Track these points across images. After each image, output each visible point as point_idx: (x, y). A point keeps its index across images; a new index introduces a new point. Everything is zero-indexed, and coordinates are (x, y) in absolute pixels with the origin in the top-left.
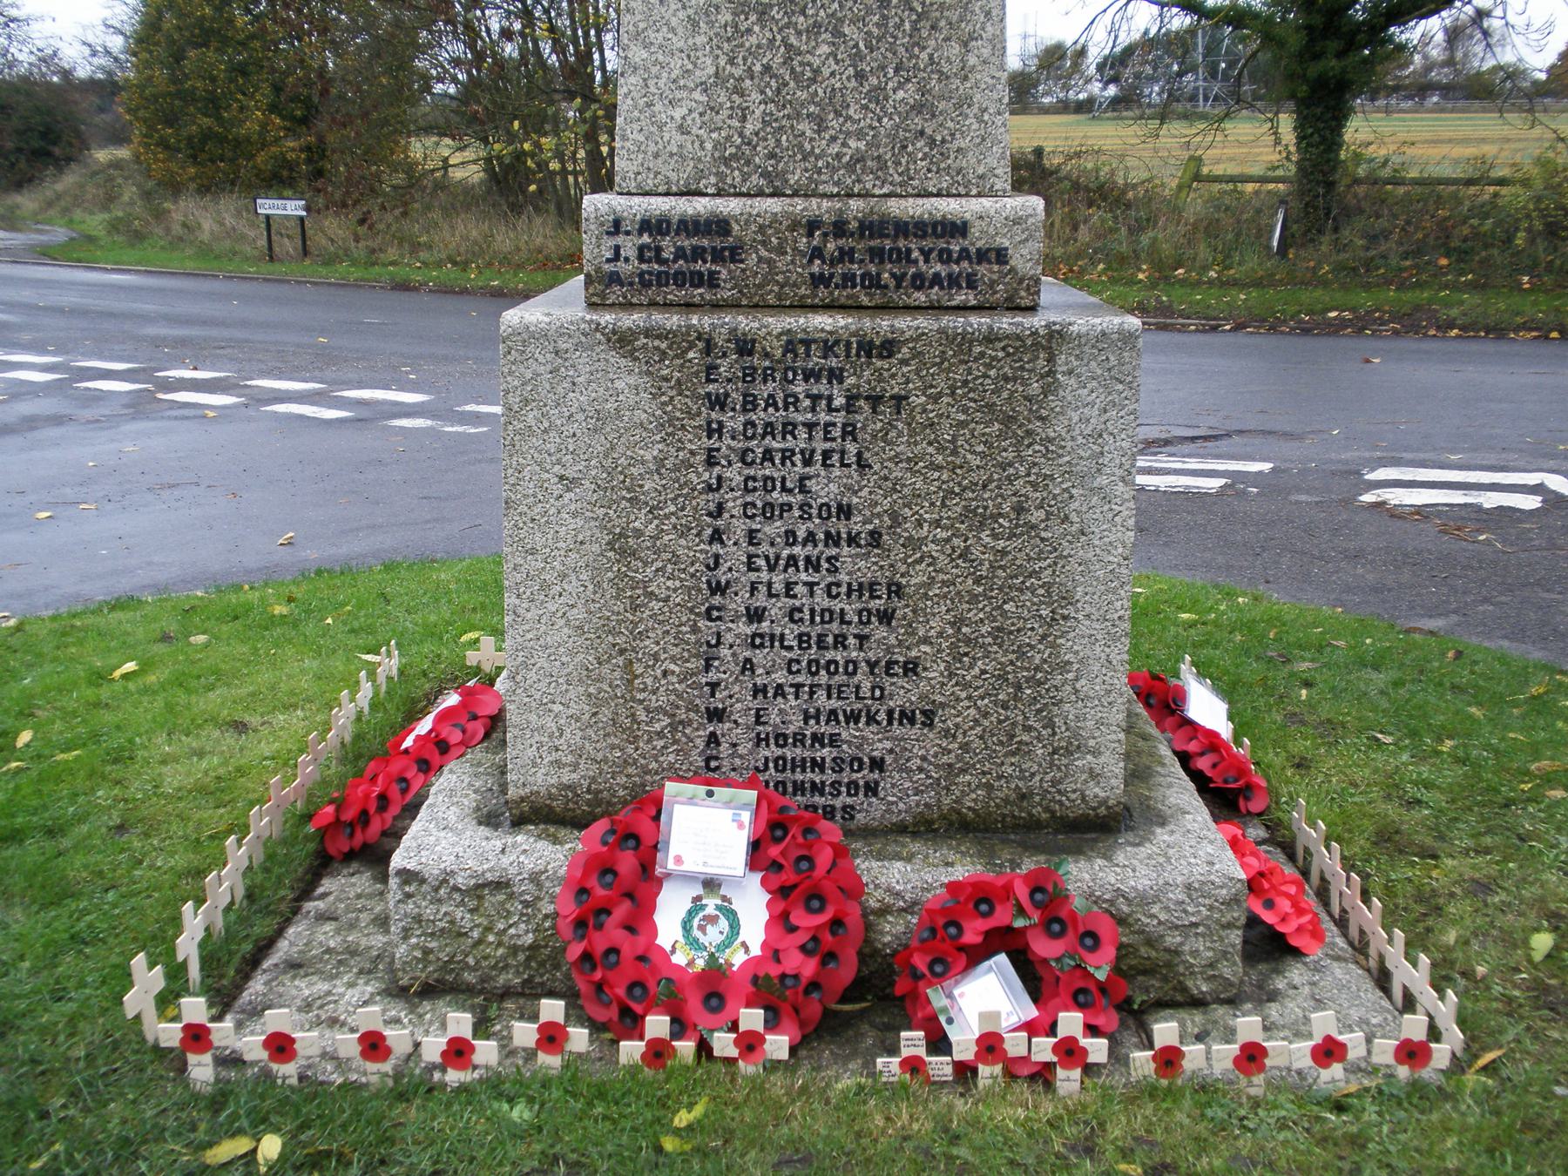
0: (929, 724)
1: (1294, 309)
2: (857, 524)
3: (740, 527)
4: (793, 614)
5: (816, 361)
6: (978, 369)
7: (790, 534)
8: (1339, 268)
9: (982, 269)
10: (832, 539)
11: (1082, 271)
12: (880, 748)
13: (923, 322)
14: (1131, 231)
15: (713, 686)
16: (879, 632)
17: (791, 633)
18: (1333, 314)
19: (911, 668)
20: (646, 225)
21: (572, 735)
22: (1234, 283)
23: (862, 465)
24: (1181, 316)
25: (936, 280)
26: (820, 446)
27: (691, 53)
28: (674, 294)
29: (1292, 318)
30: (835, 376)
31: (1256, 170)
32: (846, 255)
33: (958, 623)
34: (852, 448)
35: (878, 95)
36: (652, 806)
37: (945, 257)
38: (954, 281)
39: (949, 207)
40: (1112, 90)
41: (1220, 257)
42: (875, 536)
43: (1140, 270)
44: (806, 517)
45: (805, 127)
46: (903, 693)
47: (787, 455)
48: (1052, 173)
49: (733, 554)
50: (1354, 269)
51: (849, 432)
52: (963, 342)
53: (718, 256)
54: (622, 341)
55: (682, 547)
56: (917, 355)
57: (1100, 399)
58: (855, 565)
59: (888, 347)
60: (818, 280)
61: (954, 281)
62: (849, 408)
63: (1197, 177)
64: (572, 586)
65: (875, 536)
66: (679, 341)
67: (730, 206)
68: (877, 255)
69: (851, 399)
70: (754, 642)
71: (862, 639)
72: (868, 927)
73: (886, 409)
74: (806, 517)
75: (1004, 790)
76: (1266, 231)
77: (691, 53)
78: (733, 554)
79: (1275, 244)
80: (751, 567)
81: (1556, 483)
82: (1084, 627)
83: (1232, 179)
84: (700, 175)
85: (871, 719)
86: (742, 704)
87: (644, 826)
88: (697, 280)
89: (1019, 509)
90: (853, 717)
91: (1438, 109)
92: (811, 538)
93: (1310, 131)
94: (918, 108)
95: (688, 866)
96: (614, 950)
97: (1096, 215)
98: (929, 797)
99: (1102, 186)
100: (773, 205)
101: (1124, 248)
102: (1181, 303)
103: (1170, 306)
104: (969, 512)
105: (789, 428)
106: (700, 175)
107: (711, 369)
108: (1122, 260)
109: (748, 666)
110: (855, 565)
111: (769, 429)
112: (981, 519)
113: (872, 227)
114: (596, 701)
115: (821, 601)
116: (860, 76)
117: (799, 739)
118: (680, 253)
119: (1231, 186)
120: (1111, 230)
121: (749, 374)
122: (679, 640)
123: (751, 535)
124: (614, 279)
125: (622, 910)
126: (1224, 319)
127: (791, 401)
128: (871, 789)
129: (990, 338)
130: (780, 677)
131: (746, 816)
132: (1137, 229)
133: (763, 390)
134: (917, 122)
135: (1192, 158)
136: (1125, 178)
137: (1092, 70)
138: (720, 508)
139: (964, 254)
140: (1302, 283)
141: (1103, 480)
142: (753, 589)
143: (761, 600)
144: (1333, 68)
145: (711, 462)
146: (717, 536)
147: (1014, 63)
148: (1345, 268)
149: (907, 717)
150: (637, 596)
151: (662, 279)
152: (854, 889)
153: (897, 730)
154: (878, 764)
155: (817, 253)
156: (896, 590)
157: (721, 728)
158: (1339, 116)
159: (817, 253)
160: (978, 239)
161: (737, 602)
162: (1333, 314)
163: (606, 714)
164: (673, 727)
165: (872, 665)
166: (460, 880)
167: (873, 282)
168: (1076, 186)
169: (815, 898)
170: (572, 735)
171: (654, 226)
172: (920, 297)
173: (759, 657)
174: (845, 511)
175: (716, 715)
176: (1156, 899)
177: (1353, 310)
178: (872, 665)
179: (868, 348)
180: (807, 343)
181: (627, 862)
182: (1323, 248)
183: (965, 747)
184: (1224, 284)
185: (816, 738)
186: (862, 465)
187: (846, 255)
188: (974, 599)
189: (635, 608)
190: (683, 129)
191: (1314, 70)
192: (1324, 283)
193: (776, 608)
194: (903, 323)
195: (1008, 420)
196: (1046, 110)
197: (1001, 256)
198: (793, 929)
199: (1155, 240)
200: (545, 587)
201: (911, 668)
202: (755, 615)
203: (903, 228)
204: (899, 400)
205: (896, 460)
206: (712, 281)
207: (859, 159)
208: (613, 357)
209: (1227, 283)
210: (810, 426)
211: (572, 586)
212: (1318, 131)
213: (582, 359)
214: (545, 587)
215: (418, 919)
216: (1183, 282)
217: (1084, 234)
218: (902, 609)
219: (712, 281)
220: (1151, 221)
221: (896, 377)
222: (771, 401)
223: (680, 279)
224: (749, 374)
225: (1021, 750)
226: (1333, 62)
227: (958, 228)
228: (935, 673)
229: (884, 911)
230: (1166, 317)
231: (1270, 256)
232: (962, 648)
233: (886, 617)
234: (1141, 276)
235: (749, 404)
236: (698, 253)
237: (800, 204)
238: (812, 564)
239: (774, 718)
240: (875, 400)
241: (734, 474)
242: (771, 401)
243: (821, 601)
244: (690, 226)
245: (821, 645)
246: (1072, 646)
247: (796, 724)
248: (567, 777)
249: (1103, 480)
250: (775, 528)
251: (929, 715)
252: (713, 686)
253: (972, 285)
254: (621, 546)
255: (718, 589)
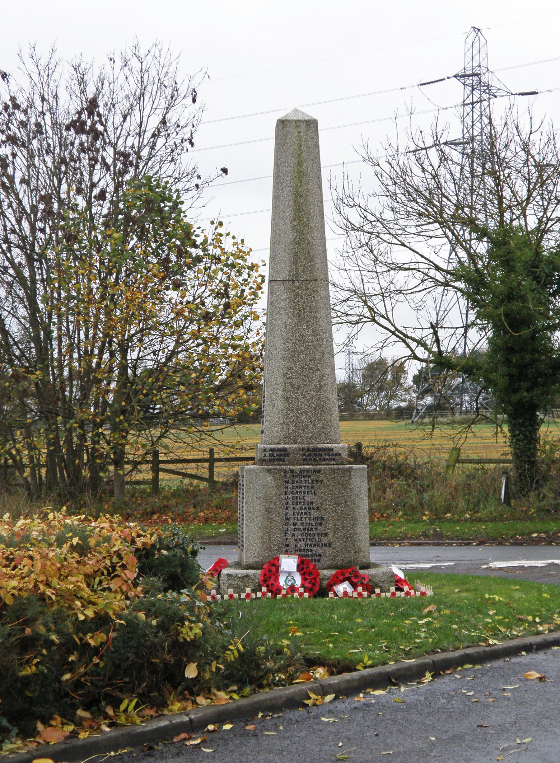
0: (330, 546)
1: (511, 533)
2: (314, 505)
3: (291, 506)
4: (302, 524)
5: (306, 474)
6: (336, 475)
7: (301, 508)
8: (540, 510)
9: (336, 457)
10: (310, 509)
11: (389, 517)
12: (320, 551)
13: (325, 467)
14: (419, 492)
15: (287, 539)
16: (319, 527)
17: (302, 528)
18: (535, 535)
19: (326, 535)
20: (271, 450)
21: (258, 551)
22: (480, 520)
23: (315, 494)
24: (448, 539)
25: (327, 459)
26: (307, 490)
27: (279, 418)
28: (276, 463)
29: (512, 538)
30: (309, 477)
31: (495, 456)
32: (310, 455)
33: (335, 525)
34: (313, 491)
35: (315, 425)
36: (278, 559)
37: (329, 455)
38: (331, 460)
39: (329, 446)
40: (429, 400)
41: (471, 506)
42: (318, 508)
43: (424, 514)
44: (304, 504)
45: (301, 431)
46: (325, 540)
47: (300, 492)
48: (368, 459)
49: (290, 512)
50: (548, 511)
51: (312, 487)
52: (333, 470)
53: (285, 455)
54: (269, 471)
55: (280, 511)
56: (324, 472)
57: (360, 480)
58: (314, 514)
59: (319, 471)
60: (304, 460)
61: (331, 460)
62: (312, 483)
63: (458, 461)
64: (259, 519)
65: (318, 508)
66: (280, 471)
67: (287, 446)
68: (316, 455)
69: (313, 481)
70: (295, 530)
71: (316, 529)
72: (321, 582)
73: (319, 483)
74: (304, 504)
75: (346, 561)
76: (497, 491)
77: (279, 418)
78: (290, 512)
79: (502, 497)
80: (294, 514)
81: (557, 561)
82: (360, 526)
83: (479, 462)
84: (280, 440)
85: (318, 546)
86: (292, 543)
87: (276, 562)
88: (281, 460)
89: (346, 502)
90: (315, 545)
91: (484, 424)
92: (305, 508)
93: (517, 432)
94: (322, 427)
95: (285, 570)
96: (272, 584)
97: (398, 483)
98: (331, 562)
99: (400, 466)
100: (295, 446)
101: (414, 502)
102: (447, 532)
103: (442, 533)
104: (336, 503)
105: (301, 487)
106: (280, 440)
107: (286, 476)
108: (413, 509)
109: (294, 535)
110: (314, 514)
111: (297, 487)
112: (338, 504)
113: (315, 449)
114: (263, 543)
115: (308, 521)
116: (311, 422)
117: (304, 550)
118: (277, 455)
119: (478, 466)
120: (406, 492)
121: (293, 476)
122: (280, 530)
123: (294, 508)
124: (264, 460)
125: (273, 578)
126: (473, 539)
127: (301, 482)
128: (319, 561)
129: (338, 469)
130: (300, 537)
131: (296, 560)
132: (422, 490)
133: (296, 480)
134: (322, 430)
135: (454, 449)
136: (415, 462)
137: (409, 382)
138: (288, 503)
139: (333, 454)
140: (519, 519)
141: (361, 496)
142: (294, 519)
143: (296, 521)
144: (525, 397)
145: (286, 494)
146: (287, 508)
147: (341, 376)
148: (543, 510)
149: (325, 545)
150: (271, 521)
151: (274, 460)
152: (318, 574)
153: (324, 548)
154: (320, 555)
155: (304, 455)
156: (322, 519)
157: (288, 548)
158: (534, 424)
159: (304, 455)
160: (335, 451)
161: (291, 522)
162: (535, 535)
163: (265, 545)
164: (279, 548)
165: (318, 534)
166: (239, 576)
167: (315, 460)
168: (384, 466)
169: (310, 573)
170: (258, 551)
171: (272, 450)
172: (324, 463)
173: (296, 533)
174: (312, 503)
175: (287, 545)
176: (377, 576)
177: (546, 532)
178: (318, 534)
179: (315, 471)
180: (304, 471)
181: (273, 569)
182: (531, 499)
183: (338, 551)
184: (473, 521)
185: (308, 550)
186: (315, 494)
187: (310, 455)
188: (338, 520)
189: (271, 523)
190: (277, 432)
191: (515, 398)
192: (532, 519)
193: (299, 523)
194: (321, 467)
195: (343, 485)
196: (370, 417)
197: (340, 455)
198: (307, 579)
199: (432, 497)
200: (253, 519)
201: (326, 535)
202: (295, 524)
203: (321, 450)
204: (322, 481)
205: (321, 493)
206: (284, 460)
207: (311, 437)
208: (267, 474)
209: (476, 520)
210: (305, 486)
211: (259, 519)
212: (521, 432)
213: (261, 474)
214: (253, 519)
215: (230, 584)
216: (450, 520)
217: (389, 494)
218: (324, 523)
219: (284, 460)
220: (430, 486)
221: (321, 477)
222: (297, 482)
223: (277, 460)
224: (293, 476)
225: (349, 552)
226: (525, 394)
227: (331, 450)
228: (331, 536)
229: (323, 579)
230: (439, 539)
231: (500, 504)
232: (336, 530)
233: (320, 524)
234: (425, 518)
235: (293, 482)
236: (281, 455)
237: (300, 446)
238: (306, 514)
239: (299, 546)
240: (317, 481)
241: (290, 496)
242: (297, 482)
243: (308, 521)
244: (279, 450)
245: (308, 530)
246: (358, 530)
247: (303, 547)
248: (257, 560)
249: (361, 496)
250: (298, 507)
251: (330, 545)
252: (287, 539)
253: (334, 460)
254: (268, 511)
255: (287, 519)
